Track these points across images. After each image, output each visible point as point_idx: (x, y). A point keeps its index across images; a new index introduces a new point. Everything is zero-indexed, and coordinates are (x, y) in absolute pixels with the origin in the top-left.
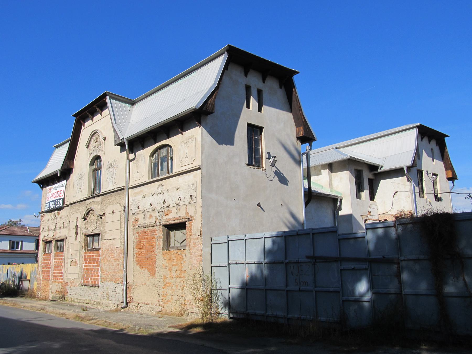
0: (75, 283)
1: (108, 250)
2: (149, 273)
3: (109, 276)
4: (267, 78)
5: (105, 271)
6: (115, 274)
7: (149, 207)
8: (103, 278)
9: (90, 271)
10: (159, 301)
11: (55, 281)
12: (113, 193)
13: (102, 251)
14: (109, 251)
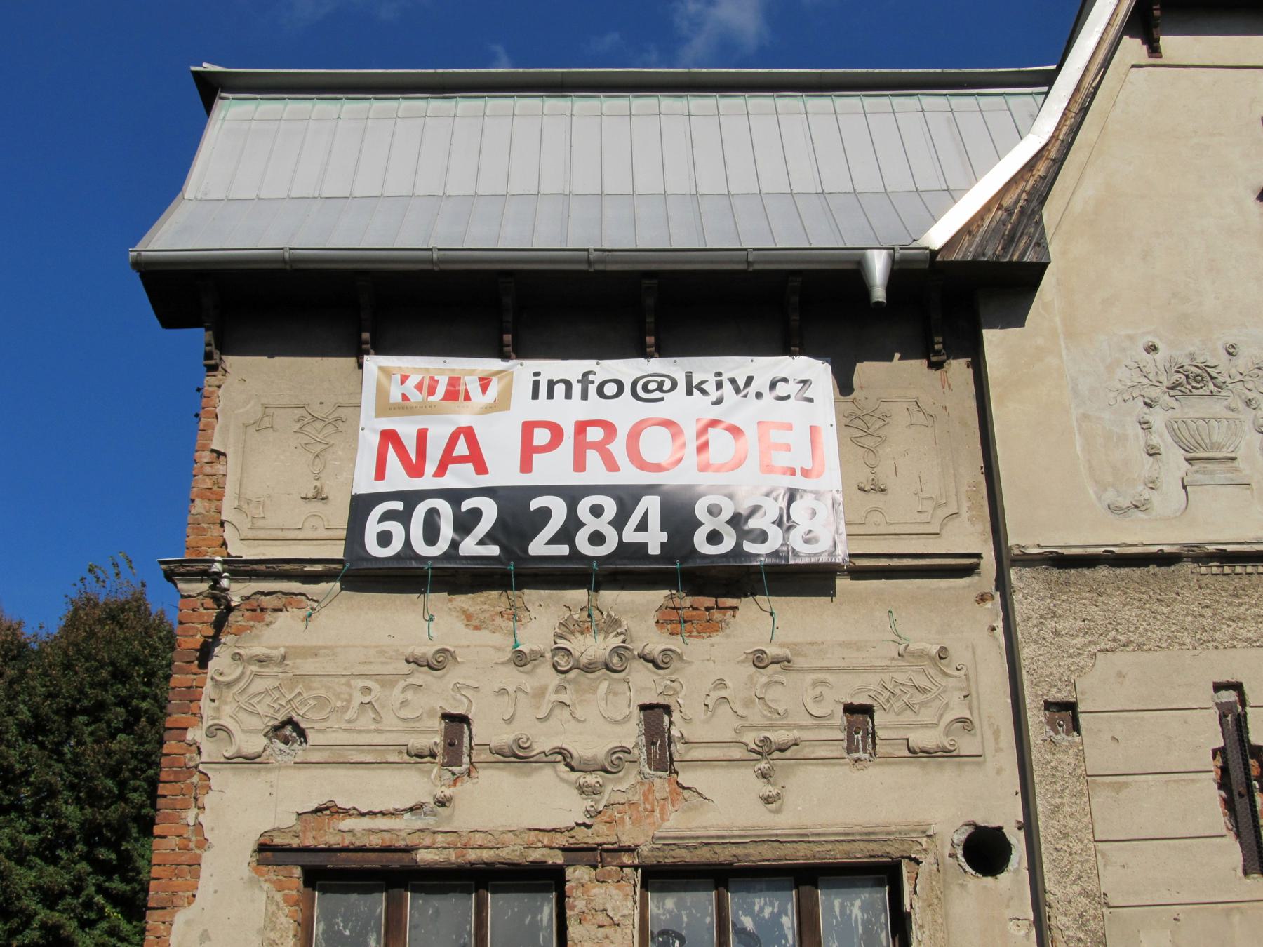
12: (1159, 566)
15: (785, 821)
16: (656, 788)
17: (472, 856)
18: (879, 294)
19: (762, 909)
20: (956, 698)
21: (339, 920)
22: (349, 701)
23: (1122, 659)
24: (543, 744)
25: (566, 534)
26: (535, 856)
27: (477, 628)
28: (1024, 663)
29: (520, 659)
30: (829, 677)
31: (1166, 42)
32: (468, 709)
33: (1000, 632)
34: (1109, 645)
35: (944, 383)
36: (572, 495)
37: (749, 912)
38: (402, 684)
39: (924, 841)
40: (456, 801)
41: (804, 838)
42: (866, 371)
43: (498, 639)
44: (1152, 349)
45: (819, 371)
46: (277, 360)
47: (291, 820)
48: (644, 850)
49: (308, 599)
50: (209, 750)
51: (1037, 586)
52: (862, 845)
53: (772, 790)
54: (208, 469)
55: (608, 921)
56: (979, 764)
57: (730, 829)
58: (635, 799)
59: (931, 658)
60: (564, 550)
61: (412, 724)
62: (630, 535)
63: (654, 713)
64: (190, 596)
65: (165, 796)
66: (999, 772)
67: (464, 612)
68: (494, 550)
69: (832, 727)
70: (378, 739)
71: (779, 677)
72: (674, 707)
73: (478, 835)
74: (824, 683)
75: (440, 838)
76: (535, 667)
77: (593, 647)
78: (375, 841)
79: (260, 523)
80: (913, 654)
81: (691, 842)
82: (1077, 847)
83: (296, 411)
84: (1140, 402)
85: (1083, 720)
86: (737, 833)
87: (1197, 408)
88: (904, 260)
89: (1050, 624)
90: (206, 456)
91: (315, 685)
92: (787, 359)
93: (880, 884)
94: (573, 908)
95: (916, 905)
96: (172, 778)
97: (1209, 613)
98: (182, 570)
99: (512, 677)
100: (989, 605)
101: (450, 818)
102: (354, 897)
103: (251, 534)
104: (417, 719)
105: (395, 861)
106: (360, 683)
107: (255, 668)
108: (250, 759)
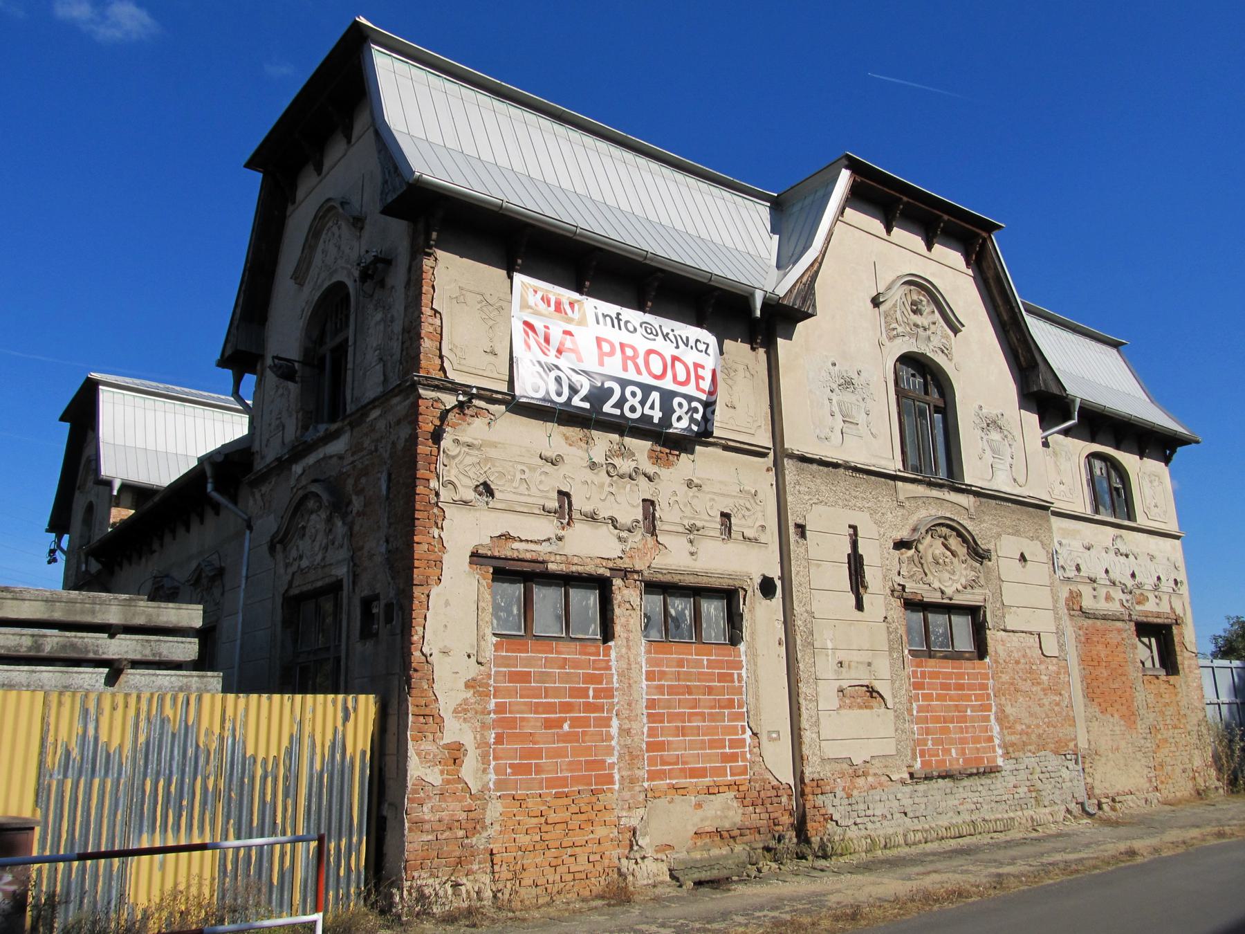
0: (875, 774)
1: (1017, 662)
2: (1122, 723)
3: (1034, 737)
4: (406, 222)
5: (1015, 722)
6: (1052, 729)
7: (1104, 575)
8: (1013, 744)
9: (951, 725)
10: (1151, 781)
11: (1223, 765)
12: (1012, 503)
13: (996, 662)
14: (1021, 666)
16: (648, 542)
17: (574, 568)
18: (758, 313)
19: (678, 606)
20: (760, 515)
21: (499, 597)
22: (514, 476)
23: (821, 508)
24: (603, 514)
25: (620, 404)
26: (601, 571)
27: (570, 445)
28: (789, 504)
29: (593, 466)
30: (716, 498)
31: (937, 247)
32: (571, 490)
33: (774, 486)
34: (816, 501)
35: (756, 358)
36: (624, 383)
37: (673, 607)
38: (539, 471)
39: (749, 580)
40: (566, 539)
41: (707, 575)
42: (728, 344)
44: (834, 364)
45: (711, 339)
46: (464, 260)
47: (488, 541)
48: (646, 573)
49: (489, 412)
50: (445, 495)
51: (793, 468)
52: (726, 580)
53: (693, 549)
54: (430, 320)
55: (631, 608)
56: (766, 547)
57: (671, 565)
58: (640, 547)
59: (752, 495)
60: (618, 412)
61: (544, 494)
62: (647, 411)
63: (649, 504)
64: (426, 399)
65: (418, 519)
66: (773, 552)
68: (587, 405)
69: (715, 522)
70: (530, 500)
71: (697, 494)
72: (656, 502)
73: (576, 558)
74: (713, 500)
75: (558, 557)
76: (599, 471)
77: (625, 466)
78: (528, 556)
79: (463, 362)
80: (746, 492)
81: (664, 571)
82: (804, 591)
83: (478, 296)
84: (829, 388)
85: (808, 533)
86: (673, 568)
87: (848, 397)
88: (770, 299)
89: (797, 487)
91: (497, 464)
92: (699, 329)
93: (722, 598)
94: (616, 599)
95: (746, 610)
96: (422, 509)
97: (848, 493)
98: (425, 382)
99: (589, 475)
100: (771, 473)
101: (563, 548)
102: (506, 585)
103: (459, 368)
104: (547, 491)
105: (538, 568)
107: (466, 449)
108: (466, 503)
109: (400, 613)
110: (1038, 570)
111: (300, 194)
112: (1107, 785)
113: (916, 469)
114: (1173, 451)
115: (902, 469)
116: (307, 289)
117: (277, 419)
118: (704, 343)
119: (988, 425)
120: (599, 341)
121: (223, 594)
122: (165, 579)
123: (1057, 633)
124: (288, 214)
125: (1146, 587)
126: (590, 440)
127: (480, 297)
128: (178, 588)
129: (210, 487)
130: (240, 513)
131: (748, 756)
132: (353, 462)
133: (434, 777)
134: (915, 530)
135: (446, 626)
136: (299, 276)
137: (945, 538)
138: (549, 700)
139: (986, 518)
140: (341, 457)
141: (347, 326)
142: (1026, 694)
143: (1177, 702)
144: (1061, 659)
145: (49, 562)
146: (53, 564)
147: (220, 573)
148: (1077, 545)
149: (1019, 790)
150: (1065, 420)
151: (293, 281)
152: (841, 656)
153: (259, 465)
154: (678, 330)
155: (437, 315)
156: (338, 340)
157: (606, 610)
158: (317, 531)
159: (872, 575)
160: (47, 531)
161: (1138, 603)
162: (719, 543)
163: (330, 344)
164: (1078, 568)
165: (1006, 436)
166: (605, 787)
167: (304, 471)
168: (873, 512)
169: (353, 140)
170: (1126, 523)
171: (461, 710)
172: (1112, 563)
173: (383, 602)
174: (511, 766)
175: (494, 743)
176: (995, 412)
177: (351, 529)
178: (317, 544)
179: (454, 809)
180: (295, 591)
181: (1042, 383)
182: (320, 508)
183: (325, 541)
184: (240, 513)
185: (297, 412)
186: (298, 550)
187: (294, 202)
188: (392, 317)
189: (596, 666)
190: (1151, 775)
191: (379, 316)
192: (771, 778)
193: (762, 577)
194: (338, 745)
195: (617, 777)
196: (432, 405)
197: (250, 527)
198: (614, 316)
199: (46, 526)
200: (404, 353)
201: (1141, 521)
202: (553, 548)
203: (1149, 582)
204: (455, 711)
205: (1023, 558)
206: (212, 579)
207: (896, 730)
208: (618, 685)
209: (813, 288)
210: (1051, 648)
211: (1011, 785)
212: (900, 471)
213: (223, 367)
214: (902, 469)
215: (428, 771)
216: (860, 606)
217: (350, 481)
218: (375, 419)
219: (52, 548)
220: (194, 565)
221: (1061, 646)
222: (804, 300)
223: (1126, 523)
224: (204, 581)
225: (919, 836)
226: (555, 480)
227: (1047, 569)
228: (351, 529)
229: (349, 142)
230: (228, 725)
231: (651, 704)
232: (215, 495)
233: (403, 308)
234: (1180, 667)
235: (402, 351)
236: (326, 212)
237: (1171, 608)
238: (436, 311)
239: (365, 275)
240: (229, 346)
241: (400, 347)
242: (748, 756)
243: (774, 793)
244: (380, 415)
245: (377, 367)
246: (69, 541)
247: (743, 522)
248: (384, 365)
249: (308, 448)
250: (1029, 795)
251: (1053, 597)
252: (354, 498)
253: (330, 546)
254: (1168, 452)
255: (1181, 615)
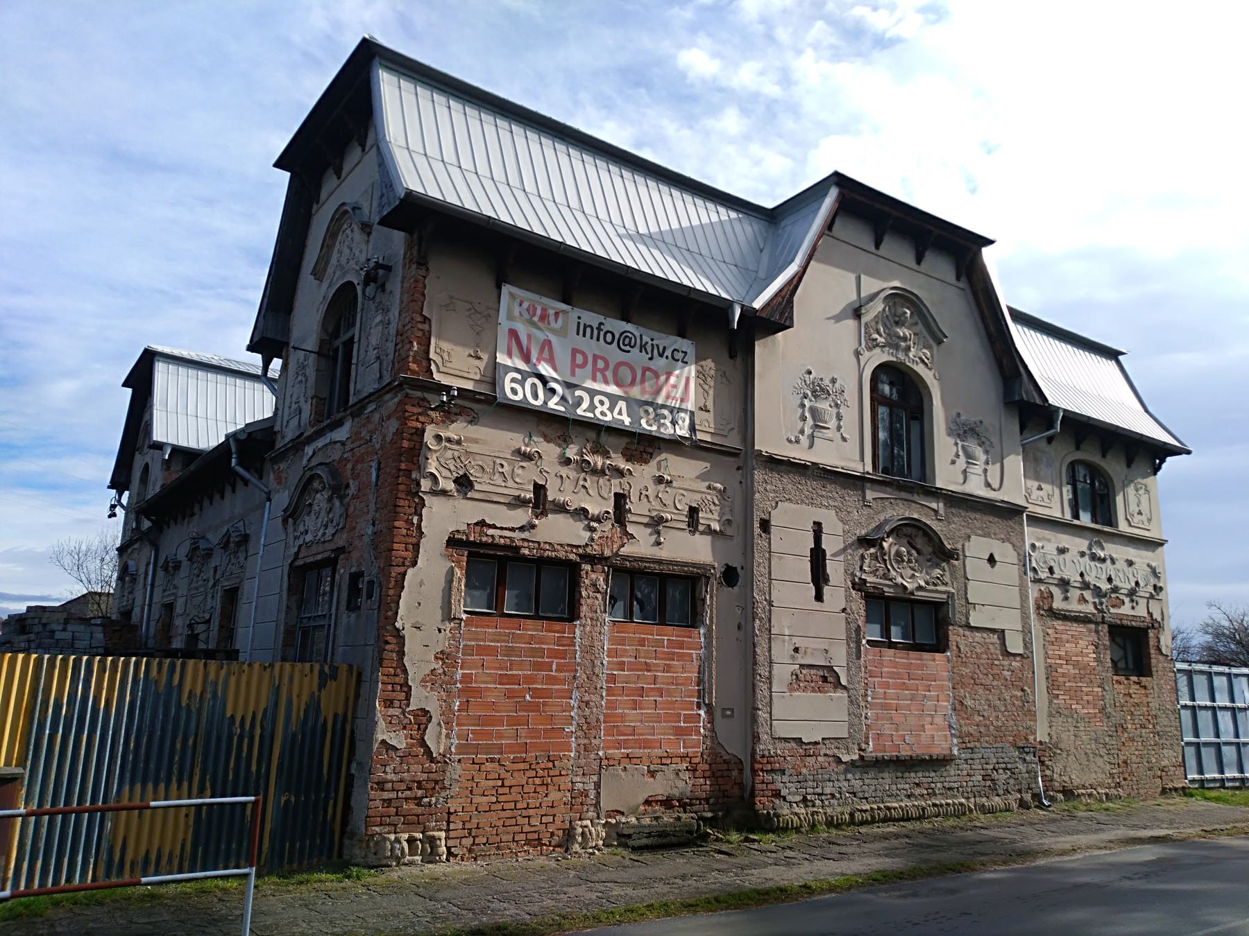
15: (663, 553)
29: (568, 462)
35: (734, 365)
43: (558, 450)
63: (620, 499)
67: (543, 433)
85: (773, 529)
90: (710, 406)
103: (444, 370)
106: (498, 461)
109: (378, 590)
110: (1008, 569)
111: (323, 196)
112: (1066, 779)
113: (885, 471)
114: (1163, 461)
115: (871, 472)
116: (325, 285)
117: (296, 403)
118: (682, 352)
119: (965, 432)
120: (575, 352)
121: (246, 559)
122: (201, 541)
123: (1023, 631)
124: (313, 212)
125: (1122, 591)
126: (567, 439)
127: (469, 306)
128: (212, 550)
129: (234, 461)
130: (263, 487)
131: (702, 730)
132: (352, 450)
133: (399, 740)
134: (879, 528)
135: (419, 604)
136: (318, 273)
137: (910, 536)
138: (514, 672)
139: (956, 519)
140: (343, 444)
141: (354, 325)
142: (987, 688)
143: (1148, 703)
144: (1025, 657)
145: (110, 516)
146: (113, 519)
147: (245, 539)
148: (1051, 549)
149: (974, 778)
150: (1048, 429)
151: (313, 277)
152: (798, 642)
153: (279, 444)
154: (657, 339)
155: (427, 321)
156: (349, 334)
157: (574, 591)
158: (320, 509)
159: (834, 569)
160: (109, 487)
161: (1113, 606)
162: (686, 534)
163: (344, 338)
164: (1051, 570)
165: (983, 443)
166: (561, 754)
167: (314, 453)
168: (838, 510)
169: (367, 149)
170: (1107, 529)
171: (431, 680)
172: (1088, 566)
173: (366, 579)
174: (474, 732)
175: (459, 710)
176: (973, 419)
177: (347, 510)
178: (320, 520)
179: (416, 771)
180: (300, 562)
181: (1026, 394)
182: (324, 488)
183: (326, 519)
184: (263, 487)
185: (312, 398)
186: (304, 525)
187: (318, 202)
188: (389, 320)
189: (561, 642)
190: (1114, 771)
191: (379, 318)
192: (724, 753)
193: (725, 567)
194: (314, 706)
195: (573, 745)
196: (418, 403)
197: (269, 499)
198: (595, 325)
199: (108, 482)
200: (397, 354)
201: (1123, 527)
202: (523, 535)
203: (1125, 586)
204: (423, 680)
205: (992, 560)
206: (239, 544)
207: (849, 714)
208: (580, 661)
209: (792, 302)
210: (1015, 646)
211: (965, 773)
212: (868, 473)
213: (252, 352)
214: (871, 472)
215: (393, 735)
216: (819, 597)
217: (349, 466)
218: (371, 412)
219: (113, 503)
220: (225, 530)
221: (1027, 644)
222: (782, 314)
223: (1107, 529)
224: (232, 545)
225: (867, 816)
226: (526, 476)
227: (1015, 570)
228: (347, 510)
229: (363, 150)
230: (209, 689)
231: (612, 678)
232: (239, 469)
233: (398, 310)
234: (1154, 669)
235: (395, 351)
236: (342, 215)
237: (1149, 612)
238: (425, 318)
239: (369, 279)
240: (257, 332)
241: (393, 348)
242: (702, 730)
243: (725, 767)
244: (376, 409)
245: (375, 365)
246: (129, 498)
247: (710, 516)
248: (380, 364)
249: (319, 434)
250: (983, 783)
251: (1021, 598)
252: (351, 482)
253: (329, 524)
254: (1158, 461)
255: (1159, 619)
